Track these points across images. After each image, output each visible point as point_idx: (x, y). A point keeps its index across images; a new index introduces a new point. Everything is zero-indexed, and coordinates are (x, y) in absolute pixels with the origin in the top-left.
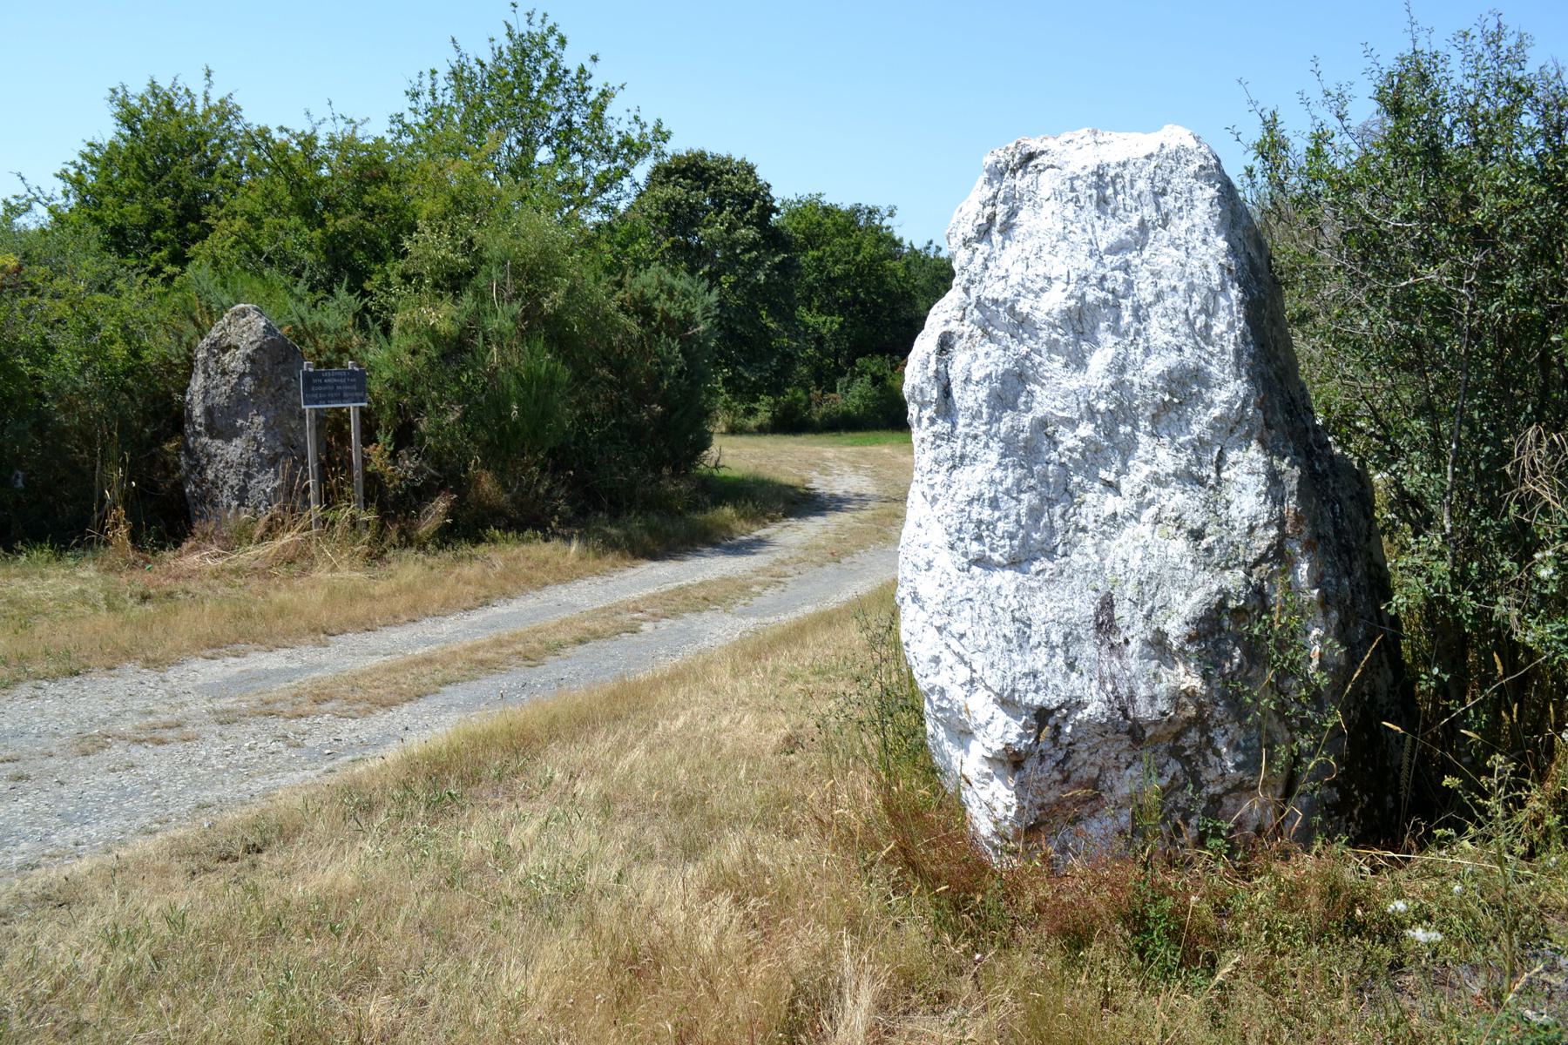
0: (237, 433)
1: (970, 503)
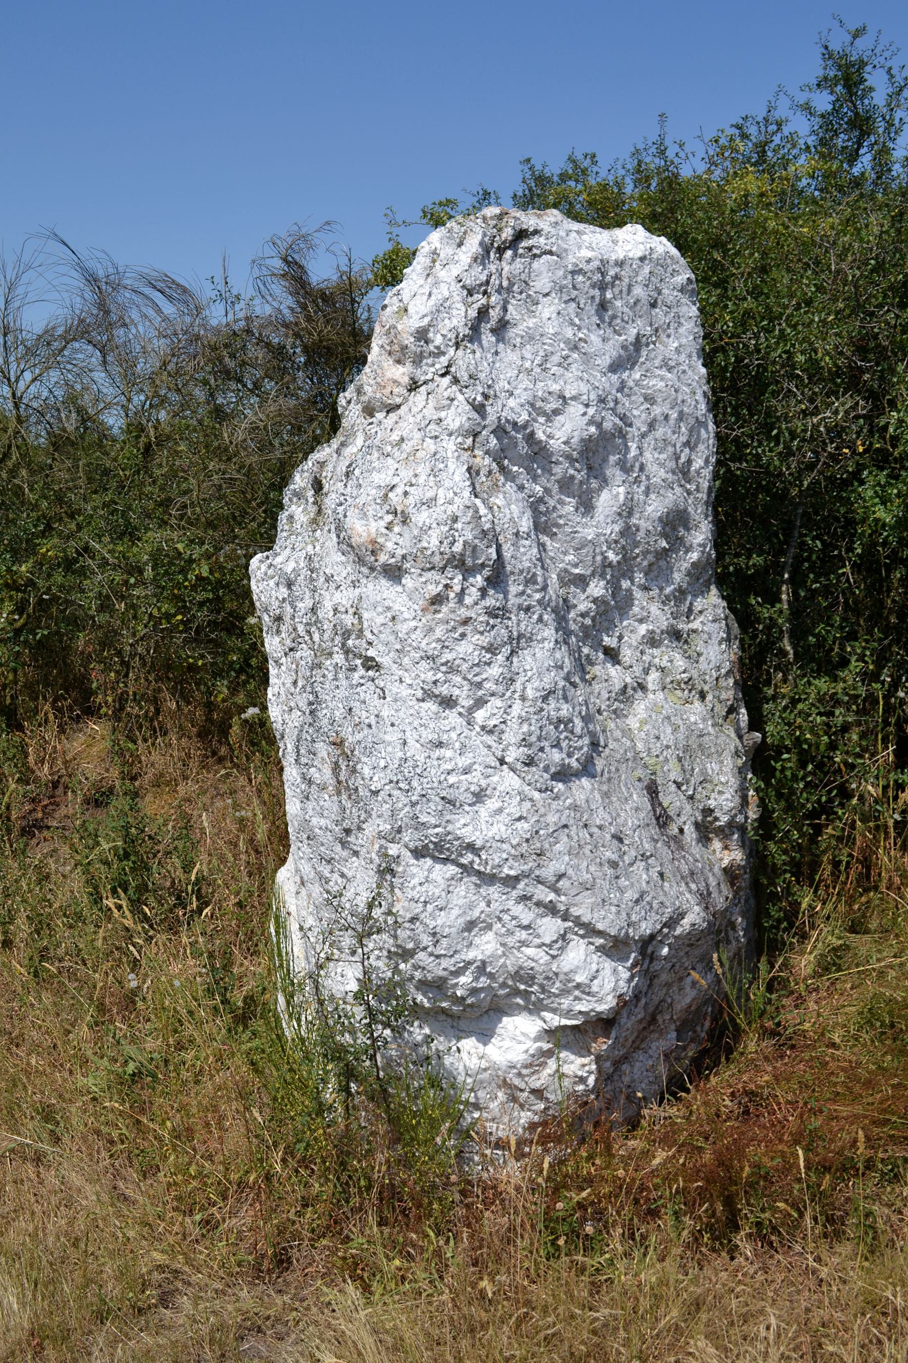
1: (545, 699)
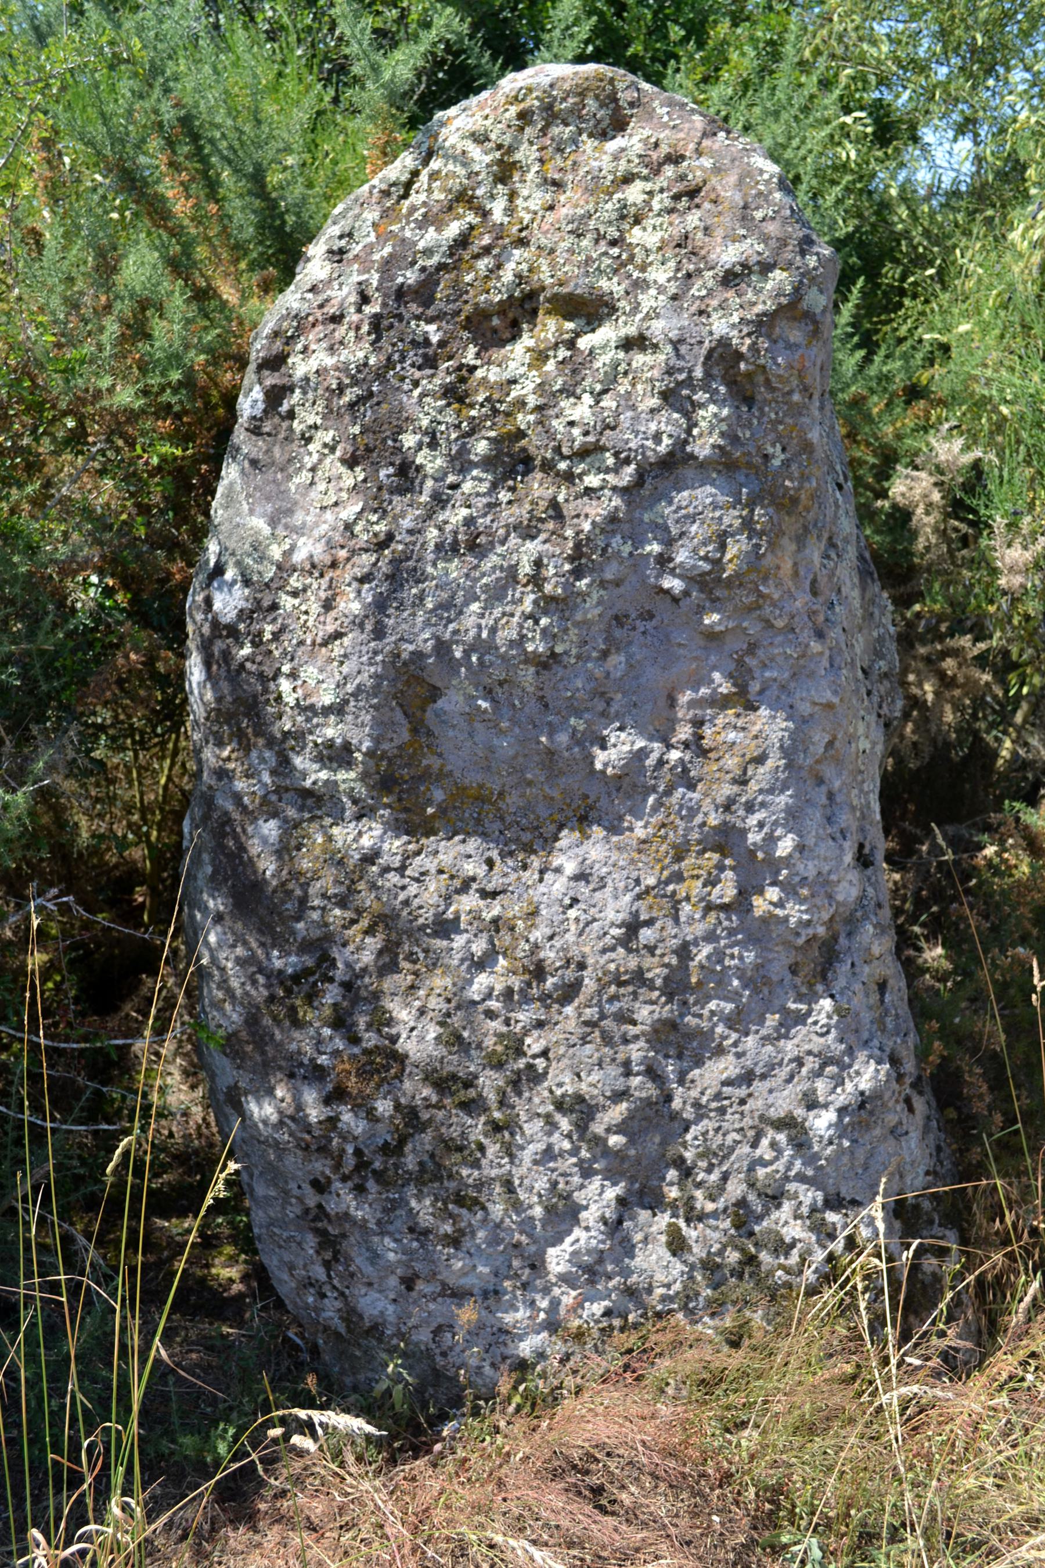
0: (593, 806)
